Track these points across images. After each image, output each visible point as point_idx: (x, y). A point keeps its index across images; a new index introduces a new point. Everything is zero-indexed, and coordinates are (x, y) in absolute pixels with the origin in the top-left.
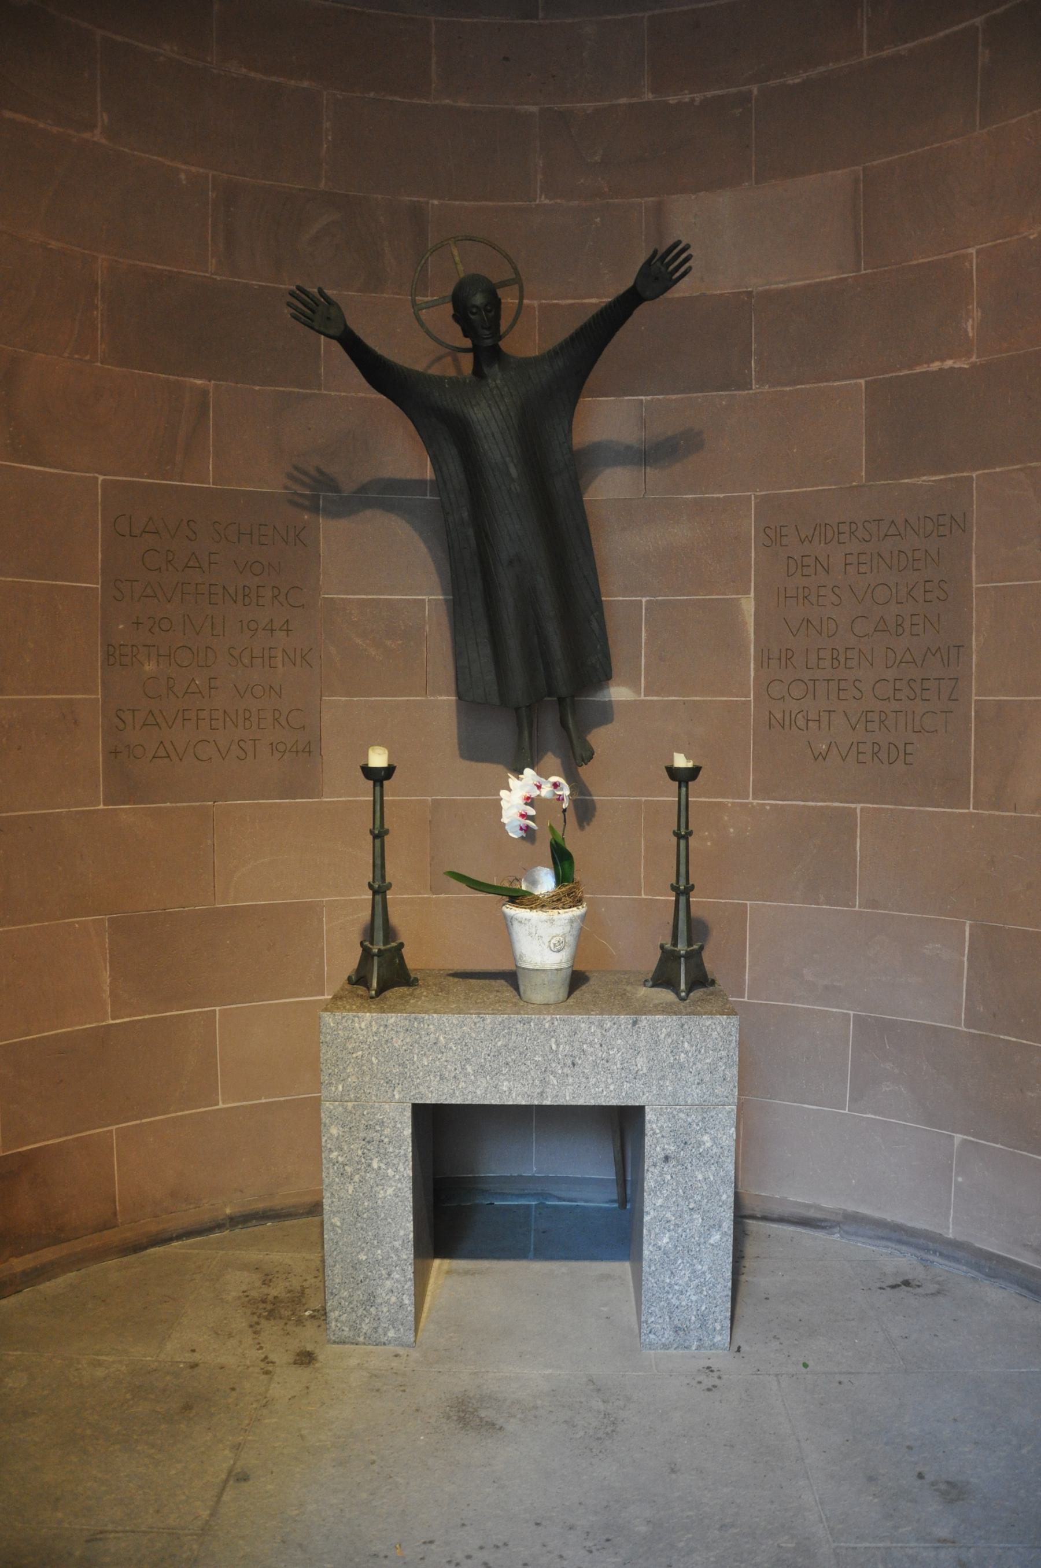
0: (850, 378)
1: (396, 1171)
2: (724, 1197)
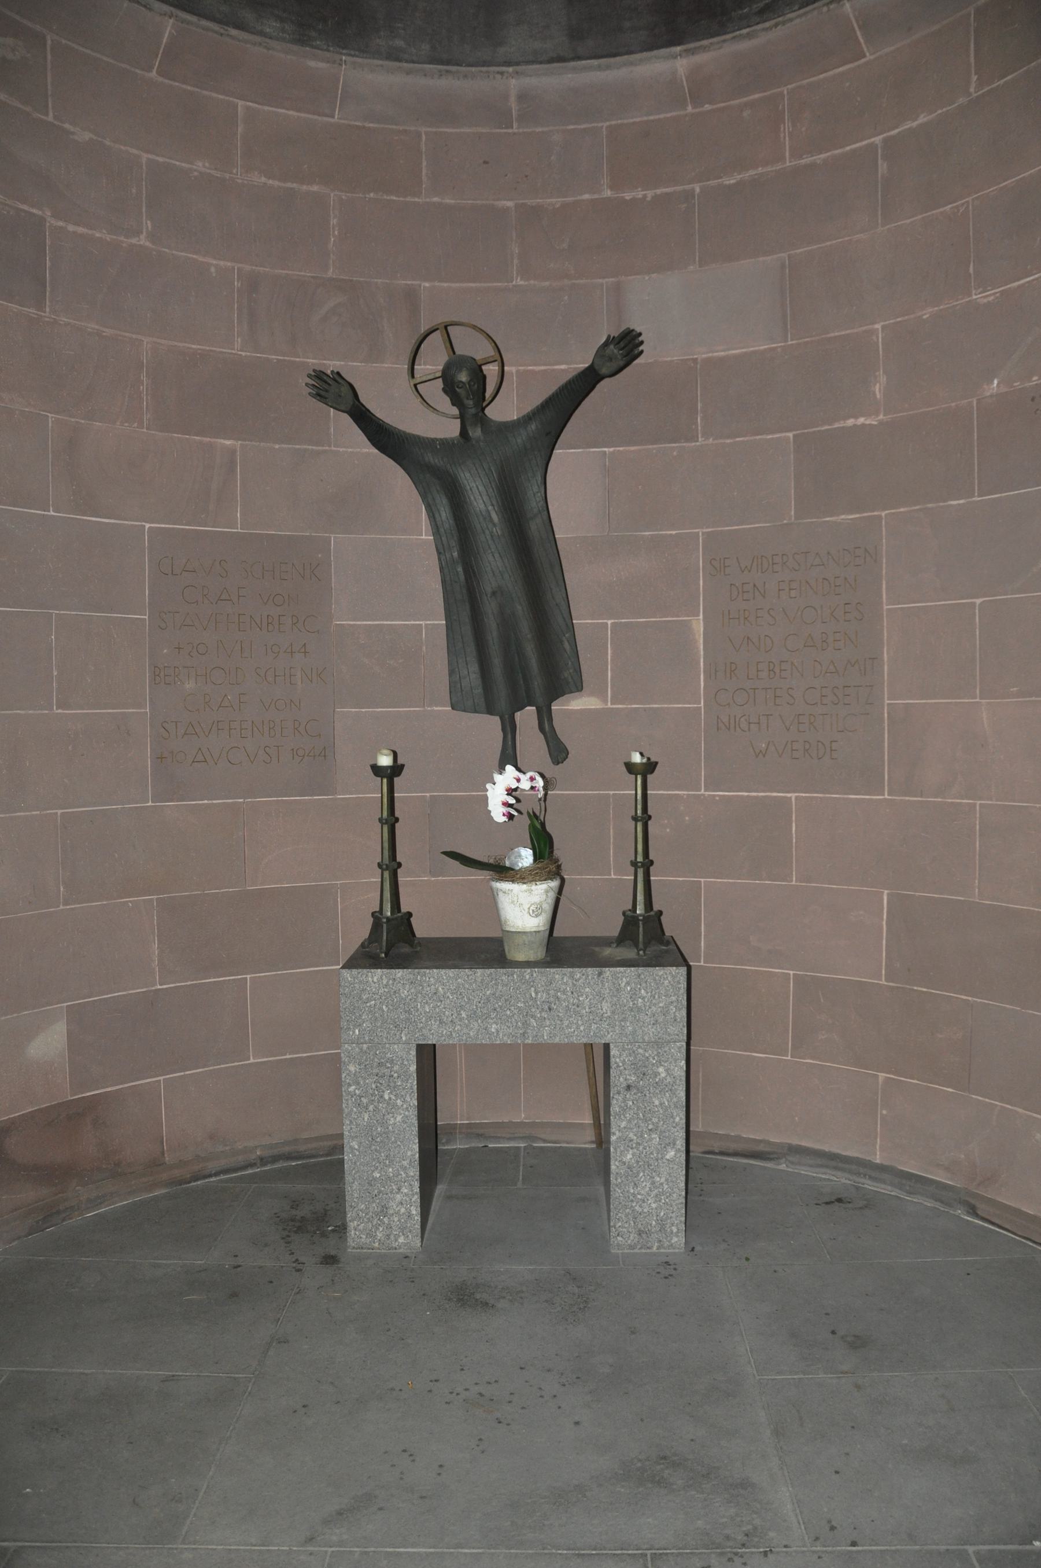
0: (781, 431)
1: (404, 1101)
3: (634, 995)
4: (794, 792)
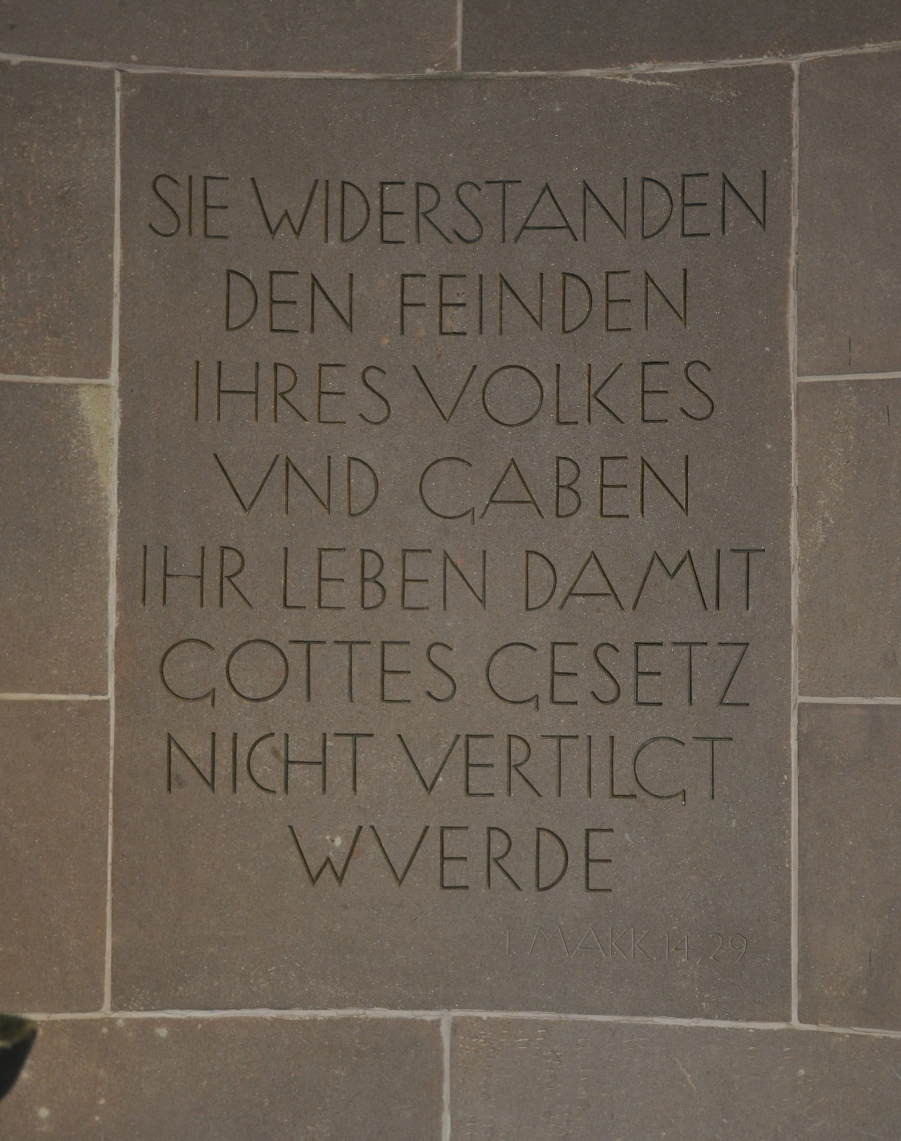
4: (448, 1004)
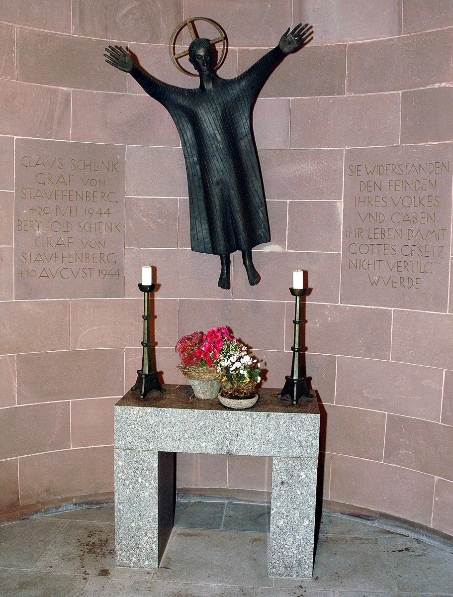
2: (311, 503)
3: (288, 429)
